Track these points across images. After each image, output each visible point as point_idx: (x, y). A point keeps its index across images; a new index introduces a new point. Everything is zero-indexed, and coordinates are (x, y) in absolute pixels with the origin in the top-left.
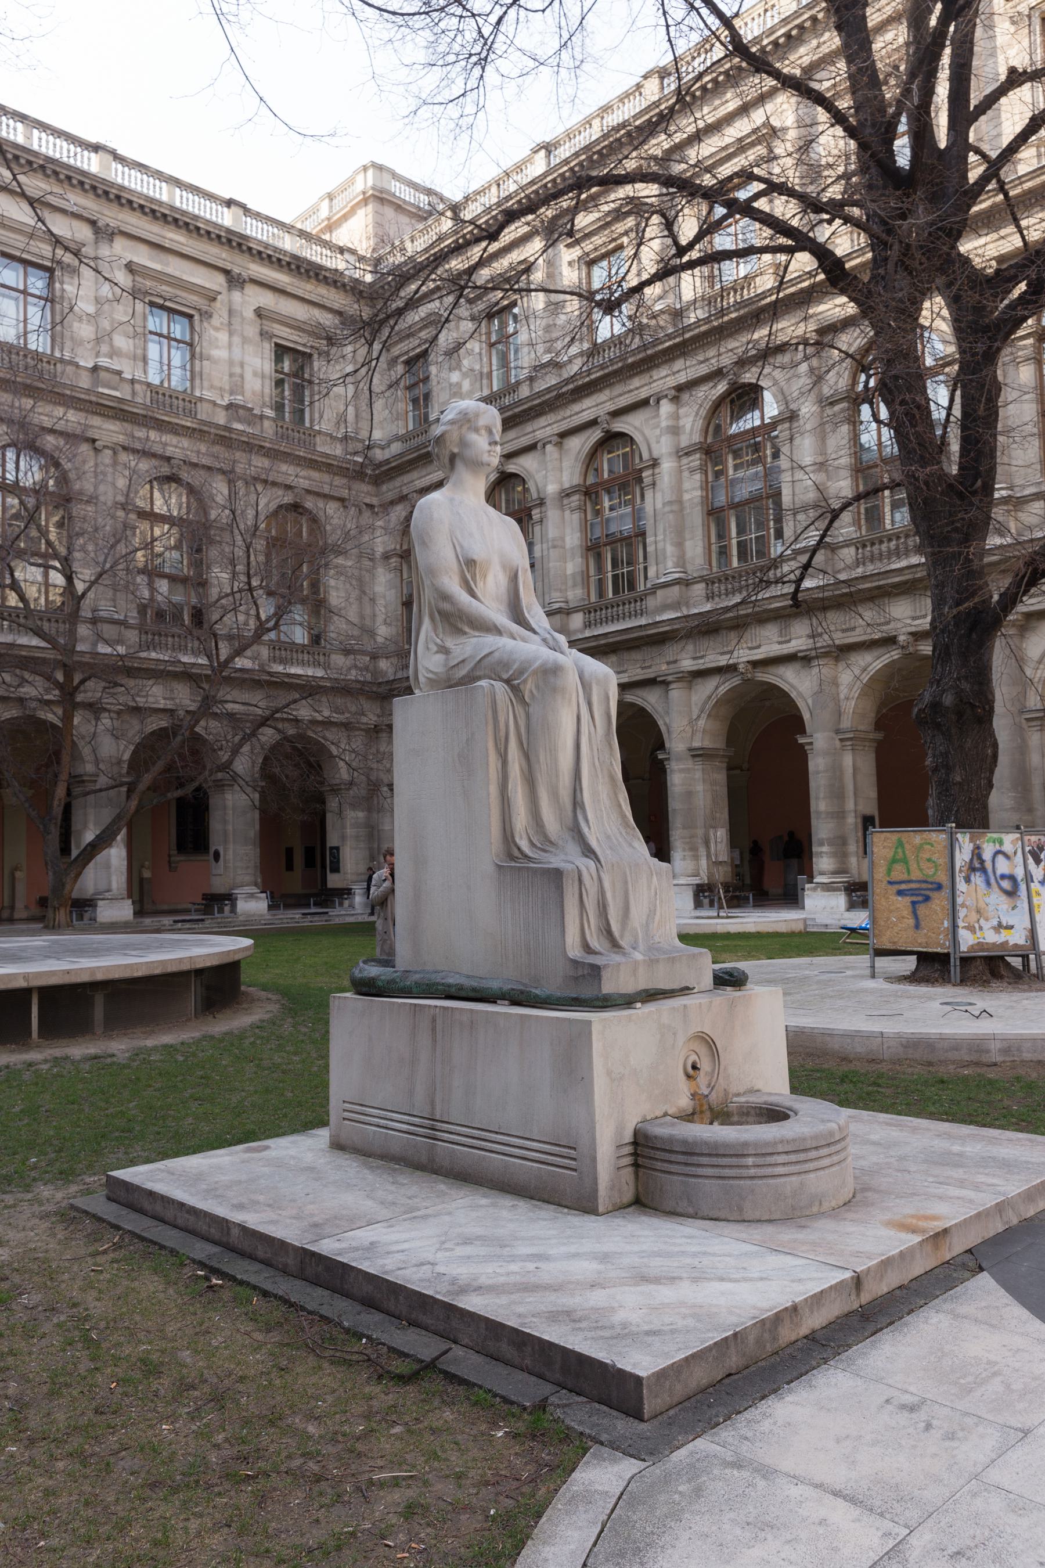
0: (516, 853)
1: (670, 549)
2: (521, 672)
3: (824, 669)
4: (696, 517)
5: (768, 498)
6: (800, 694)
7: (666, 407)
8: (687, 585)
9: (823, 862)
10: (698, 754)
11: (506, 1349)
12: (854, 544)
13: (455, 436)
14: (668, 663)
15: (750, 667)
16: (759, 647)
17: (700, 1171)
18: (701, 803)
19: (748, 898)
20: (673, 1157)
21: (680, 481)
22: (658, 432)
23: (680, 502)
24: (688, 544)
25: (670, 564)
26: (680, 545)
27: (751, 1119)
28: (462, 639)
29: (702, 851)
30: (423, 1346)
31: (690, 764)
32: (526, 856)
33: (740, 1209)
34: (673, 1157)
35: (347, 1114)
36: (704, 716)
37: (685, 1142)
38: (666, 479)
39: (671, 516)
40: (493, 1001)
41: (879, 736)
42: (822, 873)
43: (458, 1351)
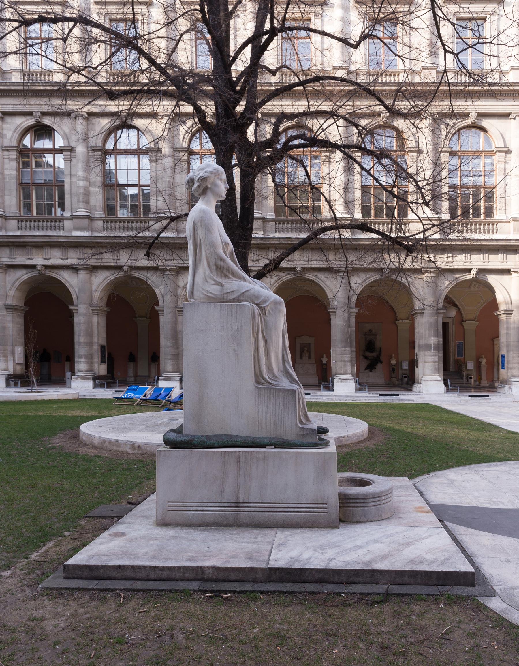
0: (263, 381)
2: (264, 301)
3: (83, 275)
4: (13, 185)
8: (6, 219)
9: (81, 366)
11: (406, 579)
12: (103, 220)
13: (211, 180)
15: (43, 268)
16: (50, 259)
18: (11, 333)
20: (358, 501)
27: (344, 483)
28: (227, 280)
29: (10, 358)
30: (382, 589)
32: (269, 383)
33: (381, 516)
35: (170, 508)
36: (14, 289)
37: (364, 495)
40: (264, 446)
41: (108, 309)
42: (79, 371)
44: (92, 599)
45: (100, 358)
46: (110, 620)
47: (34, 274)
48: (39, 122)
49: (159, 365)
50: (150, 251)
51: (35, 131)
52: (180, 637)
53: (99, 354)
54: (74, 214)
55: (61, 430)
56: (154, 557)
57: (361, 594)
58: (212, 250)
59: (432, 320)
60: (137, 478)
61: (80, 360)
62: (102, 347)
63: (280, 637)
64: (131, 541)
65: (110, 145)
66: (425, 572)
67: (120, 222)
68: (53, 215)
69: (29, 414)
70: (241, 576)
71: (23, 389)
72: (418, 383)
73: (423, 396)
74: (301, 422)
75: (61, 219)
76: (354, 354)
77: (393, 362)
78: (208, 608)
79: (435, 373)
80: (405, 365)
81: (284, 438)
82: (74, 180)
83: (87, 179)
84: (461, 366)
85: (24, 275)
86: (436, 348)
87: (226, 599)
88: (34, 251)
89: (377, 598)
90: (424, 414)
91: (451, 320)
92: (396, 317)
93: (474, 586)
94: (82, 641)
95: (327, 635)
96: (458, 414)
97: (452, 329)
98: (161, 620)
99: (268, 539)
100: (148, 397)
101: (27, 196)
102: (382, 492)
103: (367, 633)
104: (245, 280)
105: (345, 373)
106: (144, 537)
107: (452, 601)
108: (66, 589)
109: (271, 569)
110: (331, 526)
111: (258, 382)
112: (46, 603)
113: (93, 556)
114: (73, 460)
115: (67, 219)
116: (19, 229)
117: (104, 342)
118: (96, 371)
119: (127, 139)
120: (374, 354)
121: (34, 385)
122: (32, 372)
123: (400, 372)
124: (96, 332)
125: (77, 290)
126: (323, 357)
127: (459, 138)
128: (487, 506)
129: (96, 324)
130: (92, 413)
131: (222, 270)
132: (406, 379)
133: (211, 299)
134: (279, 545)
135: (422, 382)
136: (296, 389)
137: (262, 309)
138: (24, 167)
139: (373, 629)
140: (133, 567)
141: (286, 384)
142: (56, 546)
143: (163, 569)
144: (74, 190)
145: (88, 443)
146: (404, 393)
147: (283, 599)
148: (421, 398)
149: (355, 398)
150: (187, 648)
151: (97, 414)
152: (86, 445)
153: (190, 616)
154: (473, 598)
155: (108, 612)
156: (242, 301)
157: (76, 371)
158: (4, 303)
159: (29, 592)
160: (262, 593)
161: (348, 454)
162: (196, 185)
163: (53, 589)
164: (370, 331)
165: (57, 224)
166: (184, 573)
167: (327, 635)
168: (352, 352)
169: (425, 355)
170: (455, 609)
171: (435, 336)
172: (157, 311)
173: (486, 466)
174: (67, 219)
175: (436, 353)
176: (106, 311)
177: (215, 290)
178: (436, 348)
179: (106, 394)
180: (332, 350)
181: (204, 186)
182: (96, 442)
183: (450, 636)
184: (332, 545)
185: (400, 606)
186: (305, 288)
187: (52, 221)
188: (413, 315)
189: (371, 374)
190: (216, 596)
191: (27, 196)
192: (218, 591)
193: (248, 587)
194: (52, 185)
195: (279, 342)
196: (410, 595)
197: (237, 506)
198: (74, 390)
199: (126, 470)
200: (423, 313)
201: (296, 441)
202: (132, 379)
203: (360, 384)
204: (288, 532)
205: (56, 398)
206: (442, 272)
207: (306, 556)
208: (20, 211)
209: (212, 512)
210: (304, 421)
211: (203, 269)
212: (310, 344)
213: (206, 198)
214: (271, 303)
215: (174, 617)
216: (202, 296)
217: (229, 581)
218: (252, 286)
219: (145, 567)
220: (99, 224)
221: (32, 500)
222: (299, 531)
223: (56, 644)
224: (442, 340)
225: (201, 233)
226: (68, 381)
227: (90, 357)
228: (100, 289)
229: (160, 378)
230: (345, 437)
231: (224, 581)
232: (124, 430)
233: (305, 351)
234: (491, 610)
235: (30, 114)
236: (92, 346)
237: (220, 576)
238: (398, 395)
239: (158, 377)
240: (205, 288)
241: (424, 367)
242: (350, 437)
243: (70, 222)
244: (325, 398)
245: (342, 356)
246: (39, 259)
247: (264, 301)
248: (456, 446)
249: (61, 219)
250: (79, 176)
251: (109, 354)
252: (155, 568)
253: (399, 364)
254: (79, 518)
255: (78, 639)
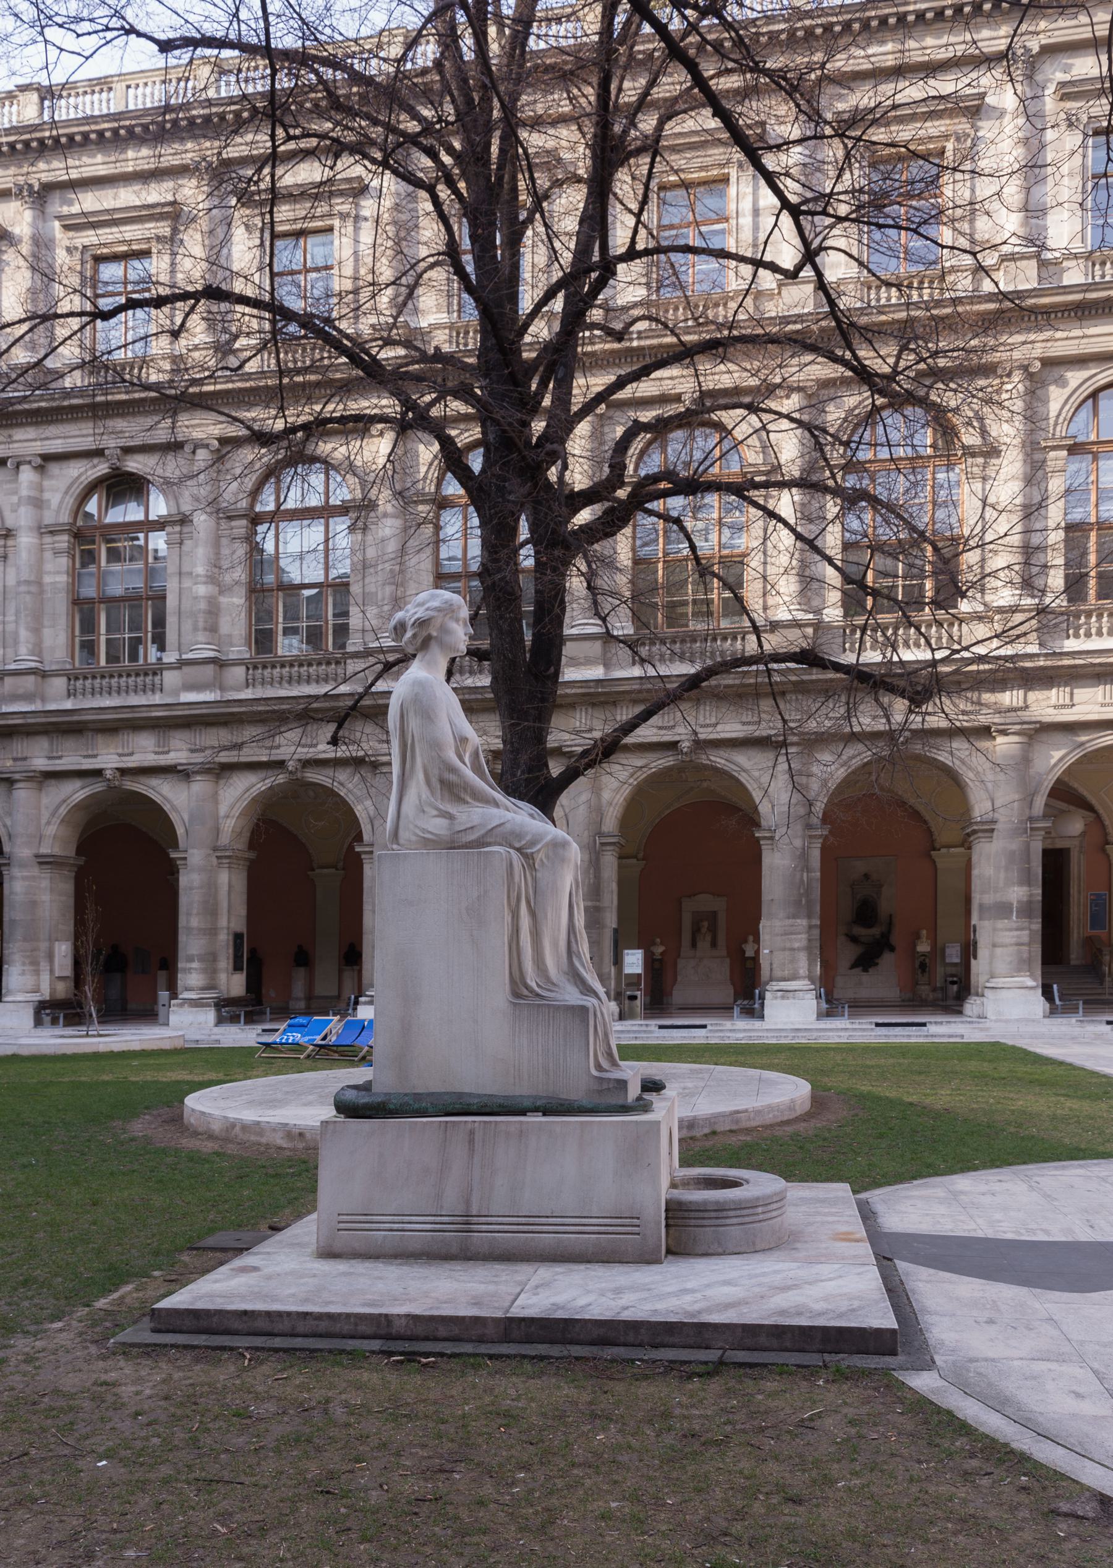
0: (526, 992)
1: (24, 634)
2: (533, 843)
3: (200, 786)
4: (59, 605)
5: (148, 599)
6: (174, 808)
7: (27, 475)
8: (44, 677)
9: (191, 977)
10: (43, 861)
11: (763, 1340)
12: (246, 664)
14: (15, 759)
15: (118, 774)
16: (132, 754)
17: (728, 1221)
19: (239, 1016)
20: (706, 1215)
21: (41, 561)
22: (15, 499)
23: (39, 583)
24: (47, 632)
25: (23, 651)
26: (37, 631)
28: (463, 808)
29: (44, 965)
30: (713, 1355)
31: (35, 871)
32: (538, 995)
33: (754, 1244)
34: (706, 1215)
35: (342, 1226)
36: (56, 821)
38: (24, 555)
39: (28, 598)
40: (523, 1113)
41: (252, 855)
42: (187, 989)
43: (728, 1353)
44: (197, 1360)
45: (231, 961)
46: (225, 1387)
47: (98, 787)
48: (118, 469)
49: (360, 971)
50: (341, 734)
51: (109, 489)
52: (339, 1412)
53: (231, 951)
54: (184, 657)
55: (147, 1108)
56: (306, 1300)
57: (671, 1362)
58: (434, 754)
59: (1015, 845)
60: (293, 1190)
61: (189, 965)
62: (238, 937)
63: (509, 1417)
64: (269, 1278)
65: (267, 503)
66: (800, 1327)
67: (283, 666)
68: (141, 662)
69: (83, 1079)
70: (456, 1331)
71: (69, 1031)
72: (977, 995)
73: (988, 1025)
74: (599, 1067)
75: (157, 670)
76: (816, 932)
77: (923, 947)
78: (392, 1377)
79: (1019, 970)
80: (953, 954)
81: (564, 1096)
82: (187, 583)
83: (212, 579)
84: (1100, 951)
85: (76, 792)
86: (1025, 910)
87: (426, 1365)
88: (100, 739)
89: (701, 1369)
90: (973, 1065)
91: (1076, 842)
92: (933, 841)
93: (895, 1354)
94: (179, 1412)
95: (594, 1416)
96: (1061, 1063)
97: (1077, 866)
98: (309, 1390)
99: (519, 1278)
100: (333, 1039)
101: (89, 625)
102: (758, 1199)
103: (666, 1415)
104: (496, 804)
105: (794, 977)
106: (292, 1273)
107: (842, 1376)
108: (155, 1345)
109: (511, 1320)
110: (648, 1258)
111: (516, 994)
112: (122, 1363)
113: (200, 1298)
114: (169, 1160)
115: (171, 667)
116: (69, 696)
117: (240, 926)
118: (223, 988)
119: (306, 489)
120: (876, 931)
121: (91, 1023)
122: (89, 995)
123: (940, 971)
124: (224, 904)
125: (186, 817)
126: (746, 941)
127: (1096, 413)
128: (1010, 1236)
129: (226, 888)
130: (213, 1076)
131: (451, 788)
132: (955, 987)
133: (430, 843)
134: (537, 1287)
135: (987, 992)
136: (589, 1004)
137: (529, 859)
138: (84, 565)
139: (677, 1411)
140: (268, 1314)
141: (572, 996)
142: (137, 1290)
143: (320, 1317)
144: (186, 605)
145: (200, 1130)
146: (939, 1019)
147: (528, 1366)
148: (982, 1030)
149: (815, 1034)
150: (347, 1425)
151: (221, 1076)
152: (196, 1134)
153: (359, 1386)
154: (886, 1372)
155: (222, 1377)
156: (489, 844)
157: (180, 989)
158: (35, 851)
159: (93, 1349)
160: (491, 1357)
161: (747, 1145)
162: (409, 634)
163: (133, 1345)
164: (866, 876)
165: (148, 679)
166: (356, 1325)
167: (594, 1416)
168: (810, 927)
169: (995, 930)
170: (845, 1387)
171: (1021, 883)
172: (359, 854)
173: (1056, 1168)
174: (171, 667)
175: (1025, 922)
176: (246, 859)
177: (437, 826)
178: (1025, 910)
179: (244, 1036)
180: (764, 925)
181: (425, 634)
182: (216, 1127)
183: (817, 1423)
184: (632, 1288)
185: (741, 1382)
186: (705, 784)
187: (137, 675)
188: (968, 835)
189: (865, 977)
190: (409, 1361)
191: (89, 625)
192: (414, 1353)
193: (468, 1348)
194: (140, 598)
195: (560, 917)
196: (765, 1365)
197: (466, 1221)
198: (176, 1029)
199: (273, 1176)
200: (992, 830)
201: (586, 1103)
202: (302, 1005)
203: (828, 1001)
204: (559, 1268)
205: (136, 1046)
206: (1042, 731)
207: (581, 1302)
208: (73, 658)
209: (419, 1233)
210: (605, 1064)
211: (417, 788)
212: (714, 915)
213: (428, 657)
214: (547, 844)
215: (332, 1387)
216: (414, 838)
217: (436, 1339)
218: (509, 815)
219: (289, 1314)
220: (238, 673)
221: (95, 1224)
222: (582, 1267)
223: (137, 1414)
224: (1040, 891)
225: (414, 724)
226: (162, 1011)
227: (210, 959)
228: (236, 812)
229: (362, 999)
230: (746, 1111)
231: (427, 1339)
232: (273, 1103)
233: (704, 930)
234: (910, 1388)
235: (99, 453)
236: (216, 934)
237: (420, 1330)
238: (924, 1025)
239: (357, 998)
240: (420, 823)
241: (992, 957)
242: (758, 1112)
243: (176, 673)
244: (741, 1035)
245: (785, 939)
246: (108, 757)
247: (533, 843)
248: (1012, 1130)
249: (157, 670)
250: (198, 576)
251: (253, 952)
252: (306, 1315)
253: (938, 951)
254: (180, 1251)
255: (172, 1410)
